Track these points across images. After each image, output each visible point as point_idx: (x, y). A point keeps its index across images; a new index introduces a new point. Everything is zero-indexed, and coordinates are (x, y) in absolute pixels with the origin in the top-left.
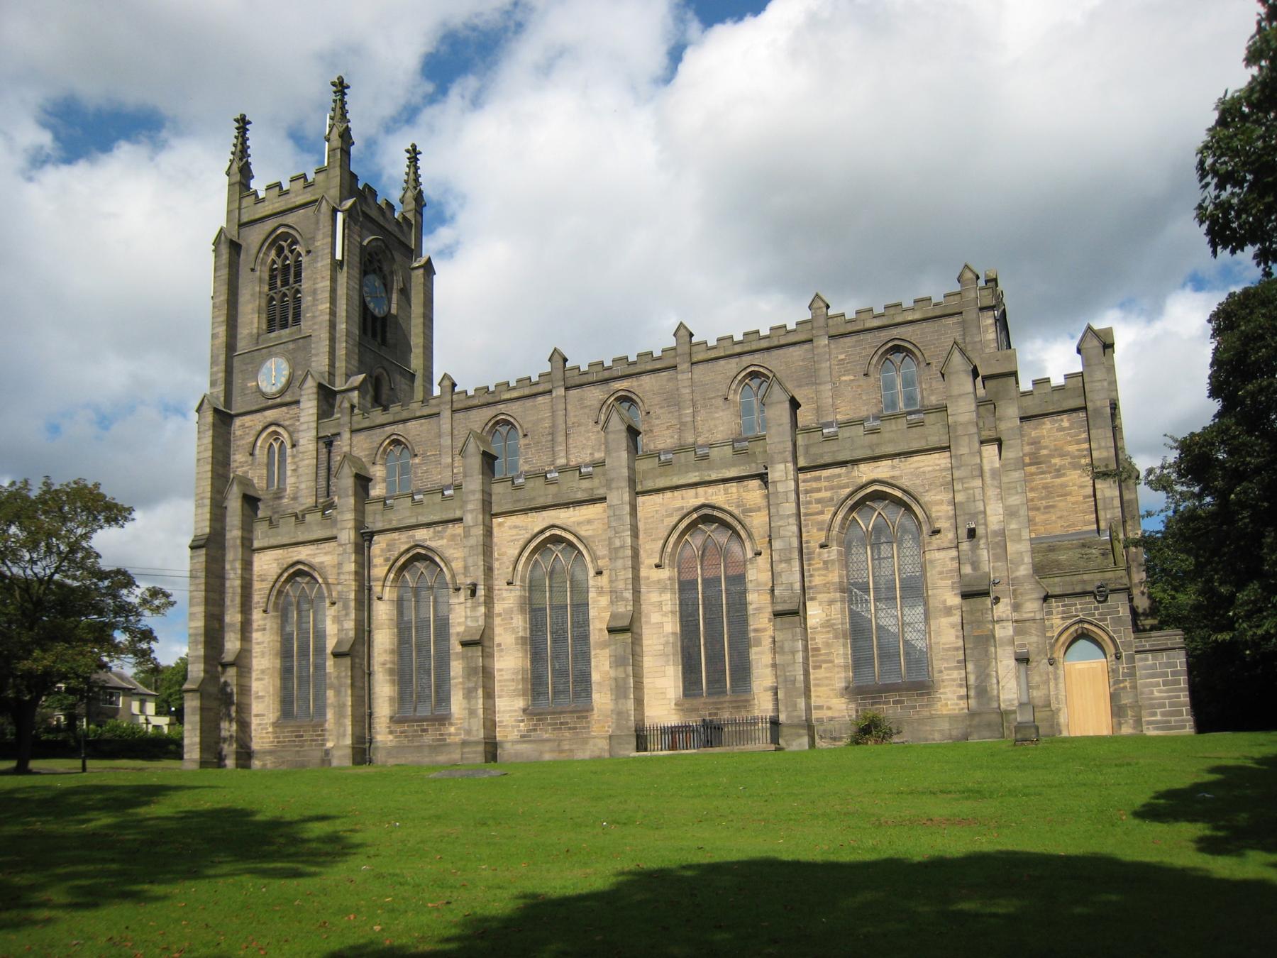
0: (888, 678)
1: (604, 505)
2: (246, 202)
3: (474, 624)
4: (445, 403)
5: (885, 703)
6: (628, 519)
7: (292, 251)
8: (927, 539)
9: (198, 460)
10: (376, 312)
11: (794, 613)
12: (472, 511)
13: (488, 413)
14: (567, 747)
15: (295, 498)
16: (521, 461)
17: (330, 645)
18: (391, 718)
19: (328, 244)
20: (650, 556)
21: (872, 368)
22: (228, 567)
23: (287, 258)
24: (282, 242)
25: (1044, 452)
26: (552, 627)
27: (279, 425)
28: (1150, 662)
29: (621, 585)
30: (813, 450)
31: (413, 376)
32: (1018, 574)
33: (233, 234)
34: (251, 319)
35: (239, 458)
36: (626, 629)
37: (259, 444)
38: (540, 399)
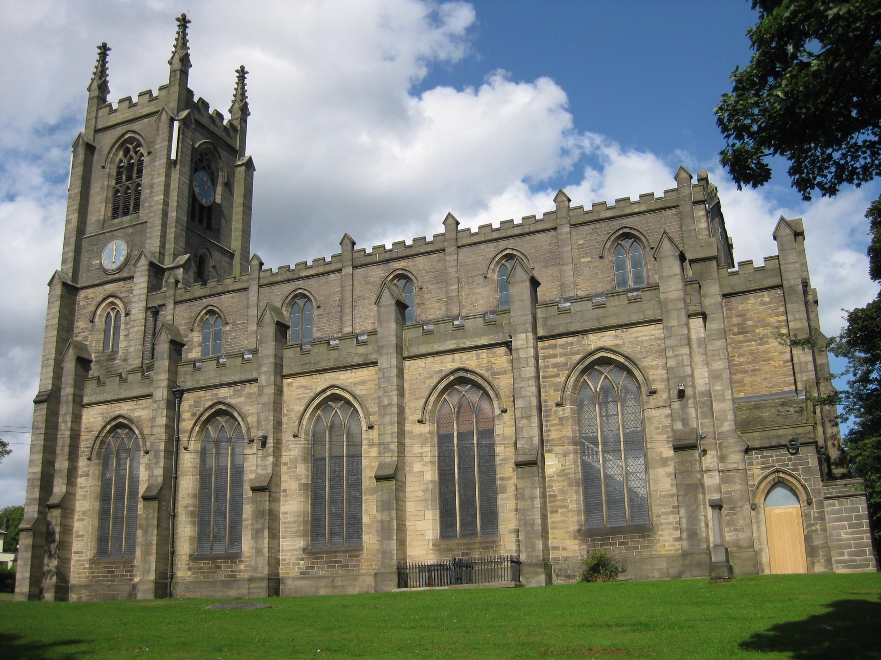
0: (616, 521)
1: (376, 368)
2: (102, 113)
3: (264, 472)
4: (253, 279)
5: (612, 544)
6: (395, 381)
7: (136, 152)
8: (645, 398)
9: (47, 326)
10: (204, 202)
11: (533, 463)
12: (265, 373)
13: (288, 288)
14: (339, 583)
15: (125, 360)
16: (315, 329)
17: (142, 489)
18: (191, 556)
19: (169, 144)
20: (414, 413)
21: (606, 252)
22: (60, 420)
23: (131, 158)
24: (129, 145)
25: (750, 323)
26: (330, 473)
27: (116, 297)
28: (837, 507)
29: (388, 439)
30: (550, 322)
31: (232, 256)
32: (723, 429)
33: (89, 138)
34: (99, 207)
35: (81, 324)
36: (392, 477)
37: (98, 313)
38: (332, 276)
